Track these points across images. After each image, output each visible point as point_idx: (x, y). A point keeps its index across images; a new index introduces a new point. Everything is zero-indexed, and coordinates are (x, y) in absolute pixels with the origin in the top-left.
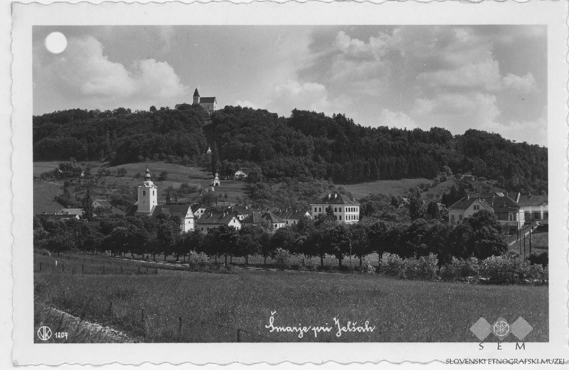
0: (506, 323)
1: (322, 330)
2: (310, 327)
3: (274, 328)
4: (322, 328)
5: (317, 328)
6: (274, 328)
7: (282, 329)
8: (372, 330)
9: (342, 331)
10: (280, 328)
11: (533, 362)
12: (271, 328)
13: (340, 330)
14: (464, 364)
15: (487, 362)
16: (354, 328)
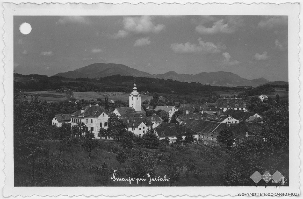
0: (270, 174)
1: (141, 180)
2: (135, 178)
3: (115, 179)
4: (141, 179)
5: (139, 179)
6: (115, 179)
7: (120, 179)
8: (168, 181)
9: (152, 181)
10: (121, 180)
11: (284, 195)
12: (114, 179)
13: (151, 180)
14: (268, 196)
15: (241, 194)
16: (158, 179)
